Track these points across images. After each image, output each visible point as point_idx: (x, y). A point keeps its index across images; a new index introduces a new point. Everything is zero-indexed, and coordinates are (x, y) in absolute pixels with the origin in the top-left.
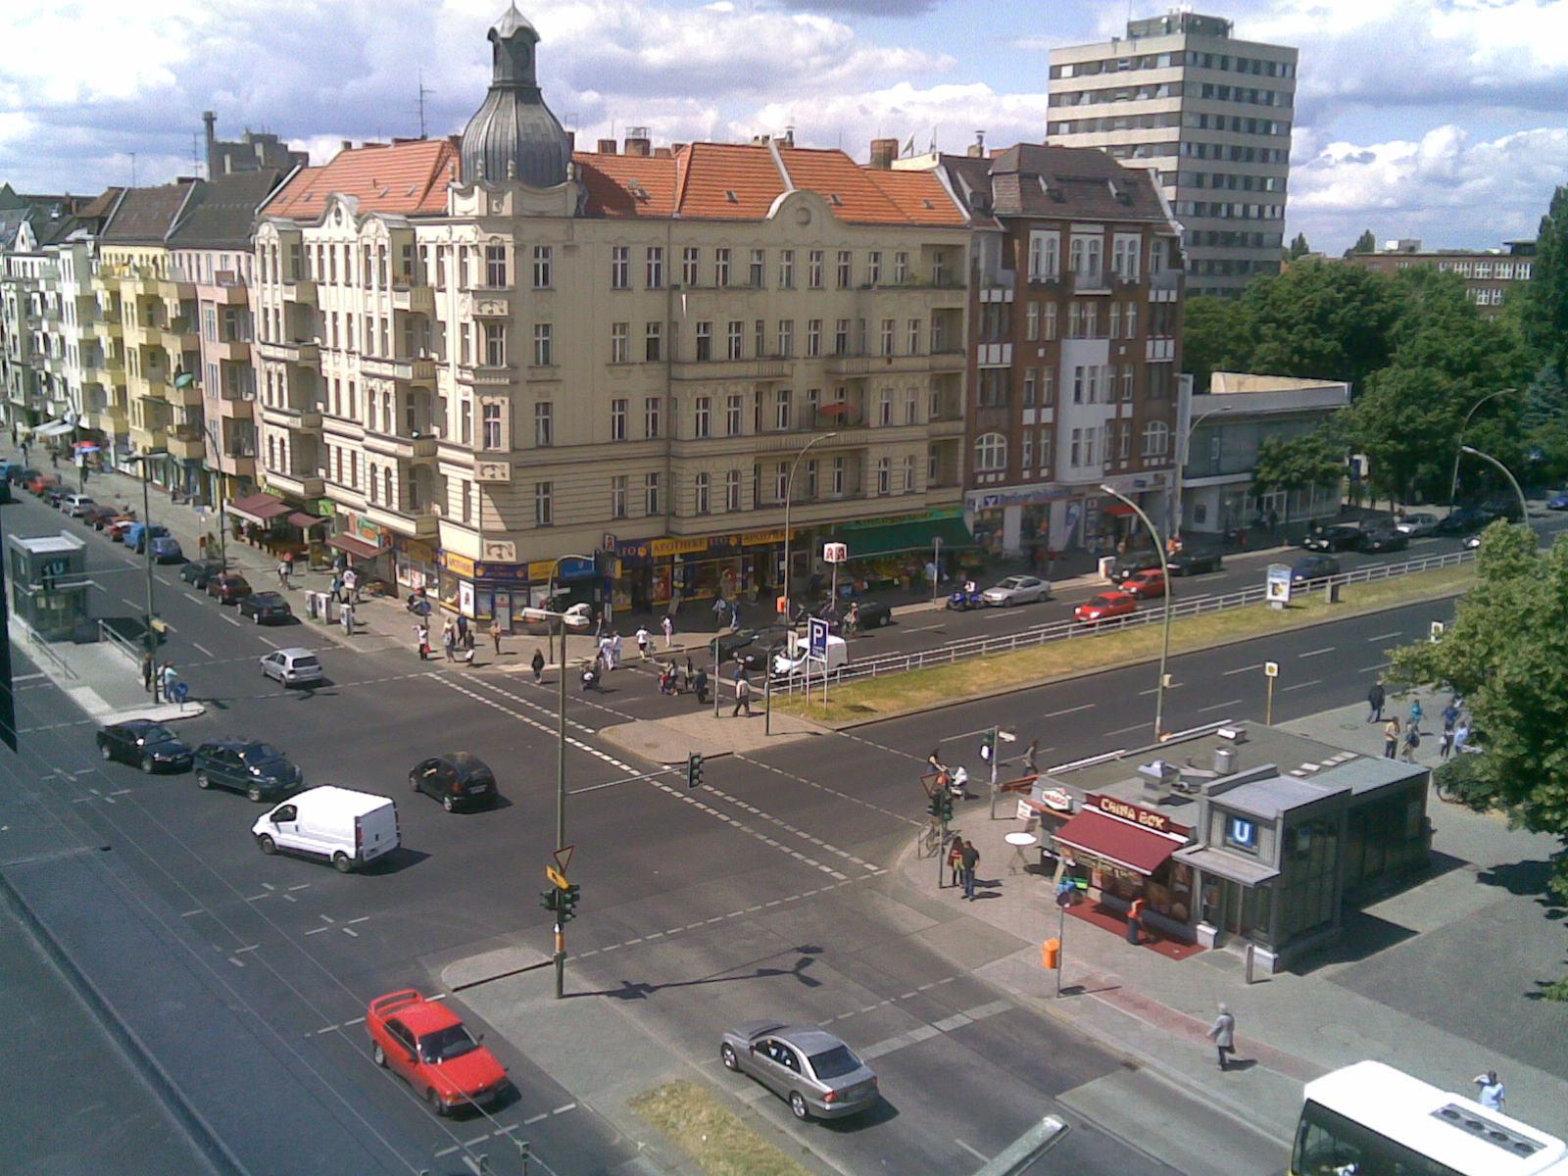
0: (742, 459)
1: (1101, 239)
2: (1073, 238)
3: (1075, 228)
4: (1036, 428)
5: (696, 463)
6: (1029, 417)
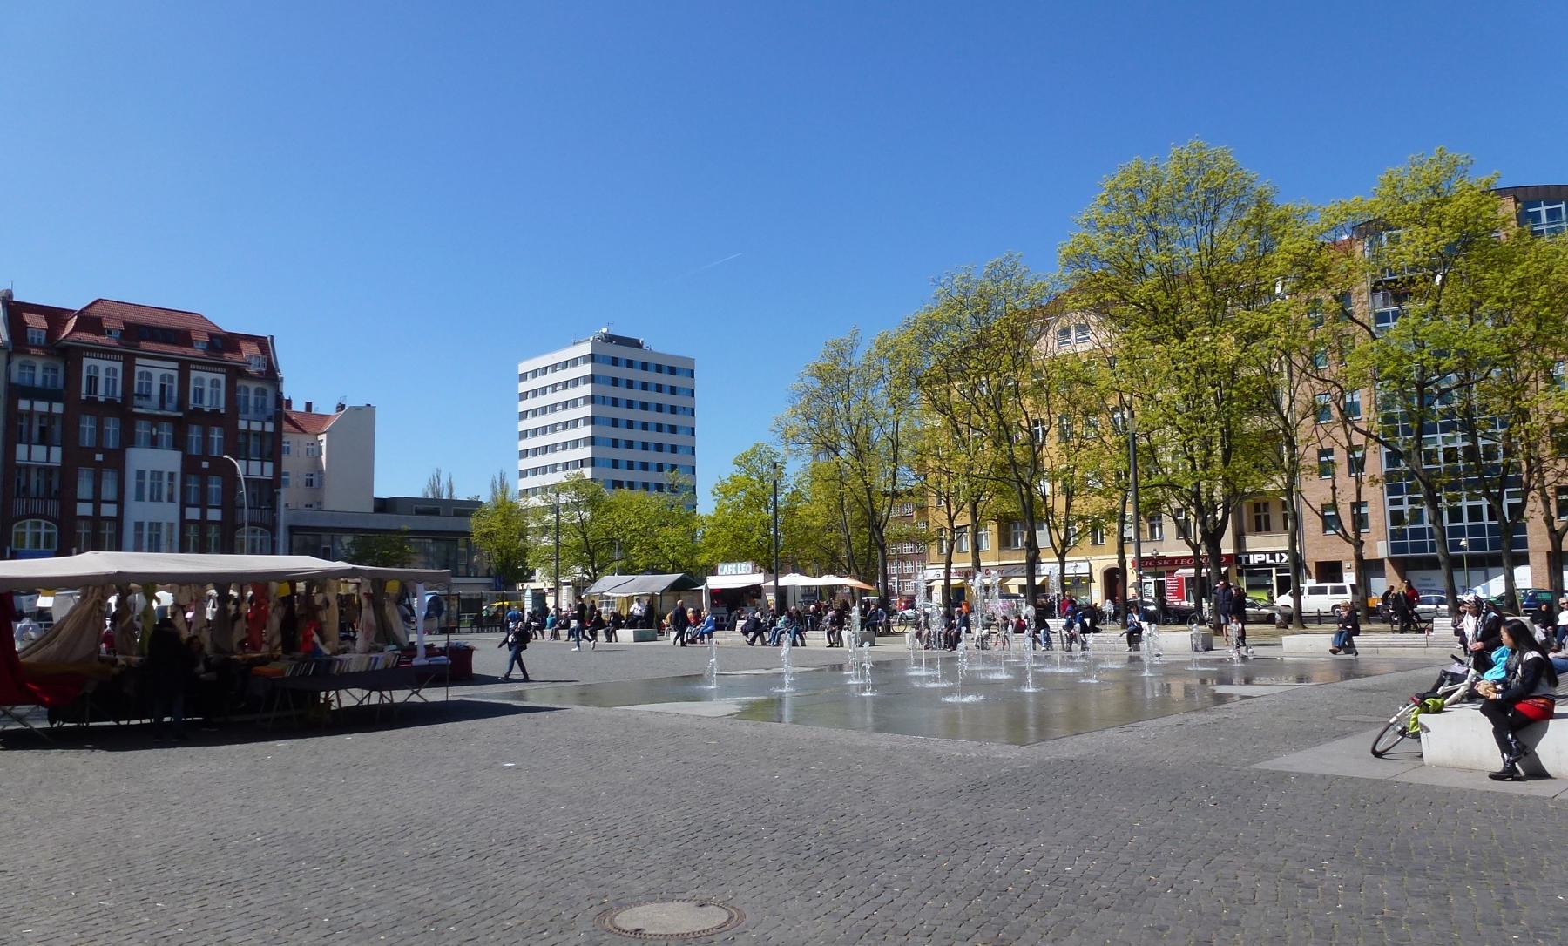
1: (175, 374)
2: (138, 370)
3: (138, 361)
6: (84, 509)
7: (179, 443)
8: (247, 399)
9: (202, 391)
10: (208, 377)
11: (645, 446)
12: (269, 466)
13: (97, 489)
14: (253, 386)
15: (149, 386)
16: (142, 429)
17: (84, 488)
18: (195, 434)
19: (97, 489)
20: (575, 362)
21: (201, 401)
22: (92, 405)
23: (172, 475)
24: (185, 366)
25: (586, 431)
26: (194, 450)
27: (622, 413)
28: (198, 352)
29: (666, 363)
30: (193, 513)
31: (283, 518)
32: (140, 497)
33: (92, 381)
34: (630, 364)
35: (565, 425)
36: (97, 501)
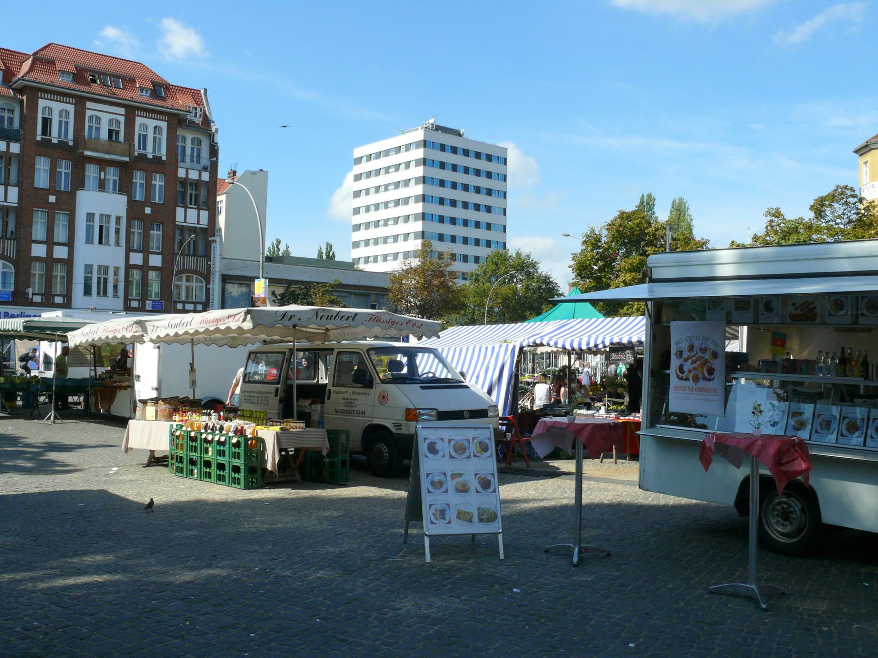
1: (122, 119)
2: (88, 113)
3: (89, 105)
4: (49, 261)
6: (38, 250)
7: (124, 187)
8: (184, 148)
9: (145, 136)
10: (151, 123)
11: (466, 223)
12: (204, 214)
13: (50, 231)
14: (189, 137)
15: (98, 129)
16: (91, 172)
17: (39, 230)
18: (139, 179)
19: (50, 231)
20: (408, 147)
21: (144, 148)
22: (46, 147)
23: (118, 219)
24: (131, 111)
25: (418, 208)
26: (139, 196)
27: (448, 193)
28: (144, 97)
29: (484, 151)
30: (137, 259)
31: (218, 267)
32: (89, 240)
33: (46, 122)
34: (454, 150)
35: (397, 203)
36: (50, 242)
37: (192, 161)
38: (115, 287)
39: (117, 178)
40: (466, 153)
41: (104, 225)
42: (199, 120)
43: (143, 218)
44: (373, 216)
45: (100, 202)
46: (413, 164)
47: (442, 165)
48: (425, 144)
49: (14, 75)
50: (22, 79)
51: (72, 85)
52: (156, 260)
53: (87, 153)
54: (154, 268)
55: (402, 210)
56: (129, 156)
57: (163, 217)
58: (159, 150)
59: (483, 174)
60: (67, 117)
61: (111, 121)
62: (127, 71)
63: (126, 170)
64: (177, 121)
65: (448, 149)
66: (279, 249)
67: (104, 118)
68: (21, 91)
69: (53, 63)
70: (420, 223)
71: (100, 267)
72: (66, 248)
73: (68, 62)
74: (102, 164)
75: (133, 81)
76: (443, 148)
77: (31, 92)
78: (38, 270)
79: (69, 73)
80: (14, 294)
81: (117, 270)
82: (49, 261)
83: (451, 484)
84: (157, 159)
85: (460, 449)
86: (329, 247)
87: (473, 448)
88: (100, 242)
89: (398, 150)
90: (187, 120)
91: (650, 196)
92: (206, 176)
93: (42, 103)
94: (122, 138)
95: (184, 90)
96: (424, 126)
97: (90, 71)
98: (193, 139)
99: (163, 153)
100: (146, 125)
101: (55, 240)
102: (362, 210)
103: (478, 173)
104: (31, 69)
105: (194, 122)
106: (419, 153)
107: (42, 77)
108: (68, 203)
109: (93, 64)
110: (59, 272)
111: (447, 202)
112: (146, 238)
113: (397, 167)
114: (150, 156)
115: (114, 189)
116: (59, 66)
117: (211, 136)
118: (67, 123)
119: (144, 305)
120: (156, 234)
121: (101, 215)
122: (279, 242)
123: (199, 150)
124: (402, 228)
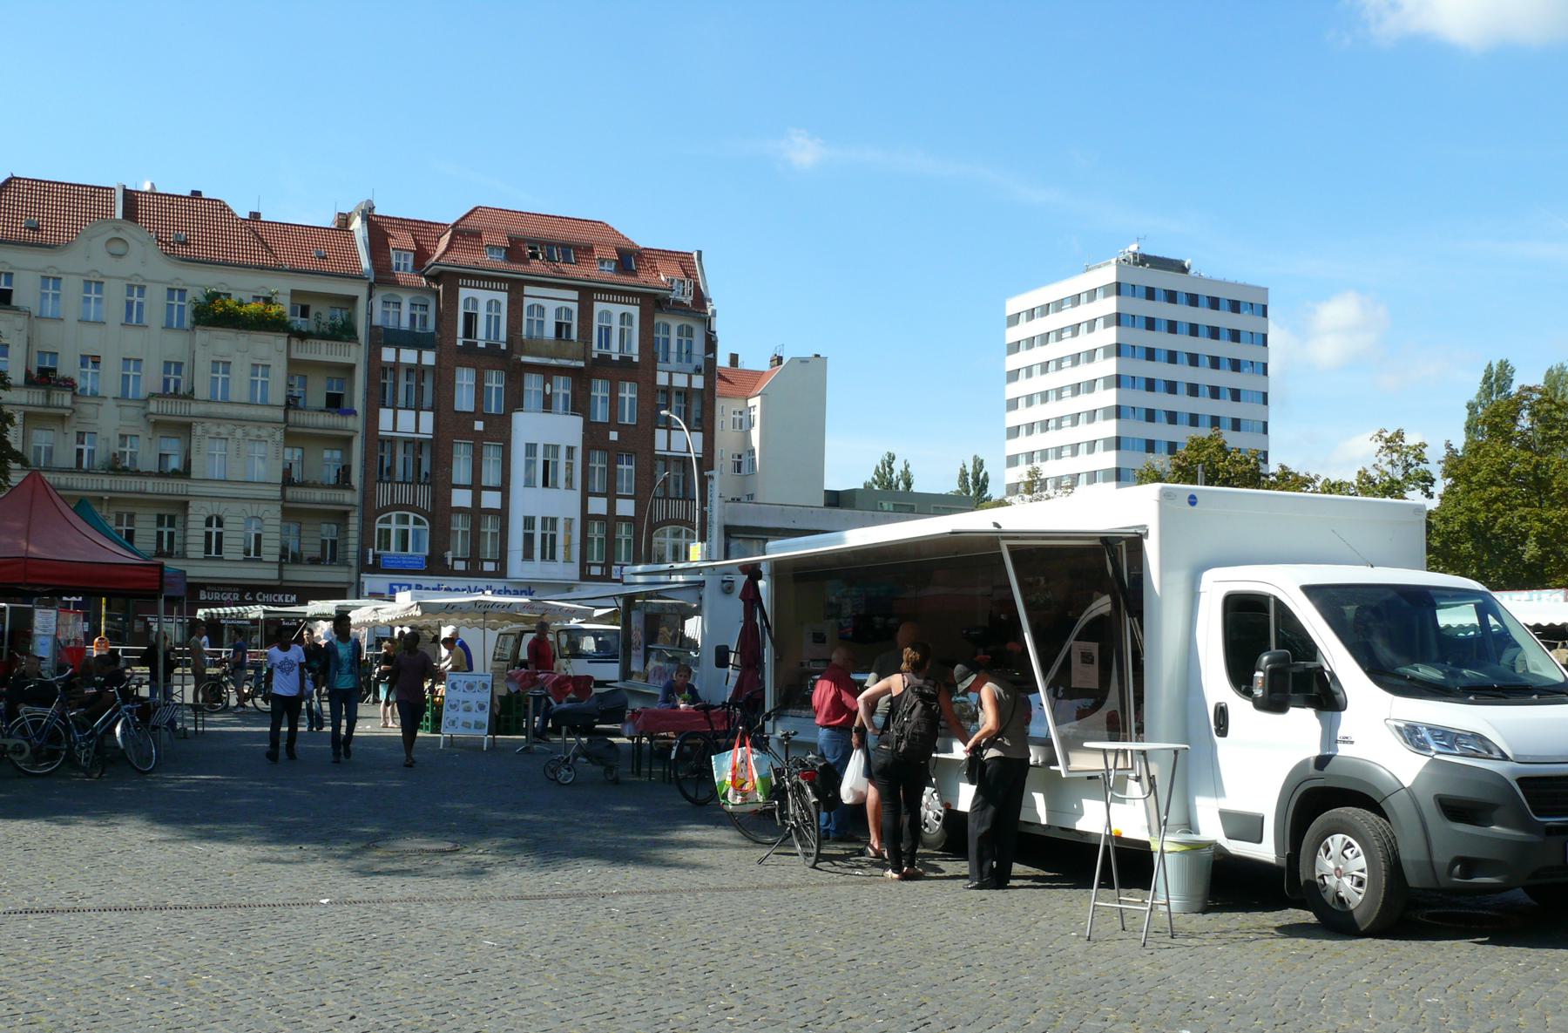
0: (264, 507)
1: (574, 307)
2: (527, 302)
3: (528, 290)
4: (476, 513)
5: (207, 504)
6: (461, 498)
7: (580, 404)
8: (667, 342)
9: (608, 329)
10: (616, 310)
14: (675, 324)
15: (541, 324)
16: (533, 385)
17: (461, 470)
18: (600, 390)
21: (607, 346)
23: (570, 450)
24: (587, 295)
26: (601, 414)
28: (601, 272)
29: (1224, 295)
33: (470, 319)
34: (1171, 297)
36: (476, 487)
37: (679, 359)
38: (568, 546)
39: (568, 392)
40: (1193, 300)
41: (551, 460)
42: (688, 300)
43: (607, 447)
44: (1039, 412)
45: (545, 428)
46: (1100, 323)
47: (1150, 324)
48: (1118, 288)
49: (430, 256)
50: (437, 263)
51: (504, 265)
52: (626, 508)
53: (525, 359)
54: (624, 519)
55: (1085, 402)
56: (584, 359)
57: (637, 442)
58: (629, 347)
59: (1224, 334)
60: (498, 309)
61: (559, 311)
62: (577, 236)
63: (579, 380)
64: (654, 303)
65: (1160, 295)
66: (892, 470)
67: (549, 307)
68: (435, 278)
69: (477, 235)
70: (1113, 422)
71: (544, 519)
72: (499, 494)
73: (499, 232)
74: (547, 372)
75: (589, 250)
76: (1150, 294)
77: (449, 280)
78: (460, 525)
79: (499, 248)
80: (429, 559)
81: (569, 522)
82: (476, 513)
83: (461, 707)
84: (626, 361)
85: (470, 687)
86: (979, 464)
87: (478, 687)
88: (545, 484)
89: (1076, 300)
90: (669, 297)
91: (1504, 365)
92: (698, 382)
93: (464, 293)
94: (574, 335)
95: (667, 255)
96: (1121, 257)
97: (529, 241)
98: (680, 328)
99: (634, 352)
100: (610, 312)
101: (484, 483)
102: (1022, 402)
103: (1214, 333)
104: (449, 247)
105: (681, 303)
106: (1109, 305)
107: (465, 258)
108: (500, 430)
109: (531, 230)
110: (489, 527)
111: (1160, 386)
112: (612, 476)
113: (1075, 329)
114: (616, 357)
115: (566, 408)
116: (486, 239)
117: (707, 322)
118: (498, 318)
119: (609, 572)
120: (626, 468)
121: (546, 446)
122: (892, 458)
123: (690, 343)
124: (1085, 432)
